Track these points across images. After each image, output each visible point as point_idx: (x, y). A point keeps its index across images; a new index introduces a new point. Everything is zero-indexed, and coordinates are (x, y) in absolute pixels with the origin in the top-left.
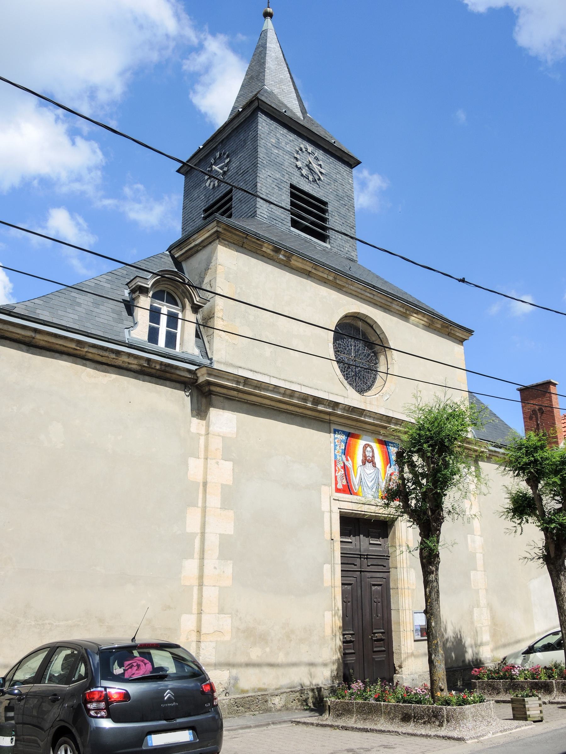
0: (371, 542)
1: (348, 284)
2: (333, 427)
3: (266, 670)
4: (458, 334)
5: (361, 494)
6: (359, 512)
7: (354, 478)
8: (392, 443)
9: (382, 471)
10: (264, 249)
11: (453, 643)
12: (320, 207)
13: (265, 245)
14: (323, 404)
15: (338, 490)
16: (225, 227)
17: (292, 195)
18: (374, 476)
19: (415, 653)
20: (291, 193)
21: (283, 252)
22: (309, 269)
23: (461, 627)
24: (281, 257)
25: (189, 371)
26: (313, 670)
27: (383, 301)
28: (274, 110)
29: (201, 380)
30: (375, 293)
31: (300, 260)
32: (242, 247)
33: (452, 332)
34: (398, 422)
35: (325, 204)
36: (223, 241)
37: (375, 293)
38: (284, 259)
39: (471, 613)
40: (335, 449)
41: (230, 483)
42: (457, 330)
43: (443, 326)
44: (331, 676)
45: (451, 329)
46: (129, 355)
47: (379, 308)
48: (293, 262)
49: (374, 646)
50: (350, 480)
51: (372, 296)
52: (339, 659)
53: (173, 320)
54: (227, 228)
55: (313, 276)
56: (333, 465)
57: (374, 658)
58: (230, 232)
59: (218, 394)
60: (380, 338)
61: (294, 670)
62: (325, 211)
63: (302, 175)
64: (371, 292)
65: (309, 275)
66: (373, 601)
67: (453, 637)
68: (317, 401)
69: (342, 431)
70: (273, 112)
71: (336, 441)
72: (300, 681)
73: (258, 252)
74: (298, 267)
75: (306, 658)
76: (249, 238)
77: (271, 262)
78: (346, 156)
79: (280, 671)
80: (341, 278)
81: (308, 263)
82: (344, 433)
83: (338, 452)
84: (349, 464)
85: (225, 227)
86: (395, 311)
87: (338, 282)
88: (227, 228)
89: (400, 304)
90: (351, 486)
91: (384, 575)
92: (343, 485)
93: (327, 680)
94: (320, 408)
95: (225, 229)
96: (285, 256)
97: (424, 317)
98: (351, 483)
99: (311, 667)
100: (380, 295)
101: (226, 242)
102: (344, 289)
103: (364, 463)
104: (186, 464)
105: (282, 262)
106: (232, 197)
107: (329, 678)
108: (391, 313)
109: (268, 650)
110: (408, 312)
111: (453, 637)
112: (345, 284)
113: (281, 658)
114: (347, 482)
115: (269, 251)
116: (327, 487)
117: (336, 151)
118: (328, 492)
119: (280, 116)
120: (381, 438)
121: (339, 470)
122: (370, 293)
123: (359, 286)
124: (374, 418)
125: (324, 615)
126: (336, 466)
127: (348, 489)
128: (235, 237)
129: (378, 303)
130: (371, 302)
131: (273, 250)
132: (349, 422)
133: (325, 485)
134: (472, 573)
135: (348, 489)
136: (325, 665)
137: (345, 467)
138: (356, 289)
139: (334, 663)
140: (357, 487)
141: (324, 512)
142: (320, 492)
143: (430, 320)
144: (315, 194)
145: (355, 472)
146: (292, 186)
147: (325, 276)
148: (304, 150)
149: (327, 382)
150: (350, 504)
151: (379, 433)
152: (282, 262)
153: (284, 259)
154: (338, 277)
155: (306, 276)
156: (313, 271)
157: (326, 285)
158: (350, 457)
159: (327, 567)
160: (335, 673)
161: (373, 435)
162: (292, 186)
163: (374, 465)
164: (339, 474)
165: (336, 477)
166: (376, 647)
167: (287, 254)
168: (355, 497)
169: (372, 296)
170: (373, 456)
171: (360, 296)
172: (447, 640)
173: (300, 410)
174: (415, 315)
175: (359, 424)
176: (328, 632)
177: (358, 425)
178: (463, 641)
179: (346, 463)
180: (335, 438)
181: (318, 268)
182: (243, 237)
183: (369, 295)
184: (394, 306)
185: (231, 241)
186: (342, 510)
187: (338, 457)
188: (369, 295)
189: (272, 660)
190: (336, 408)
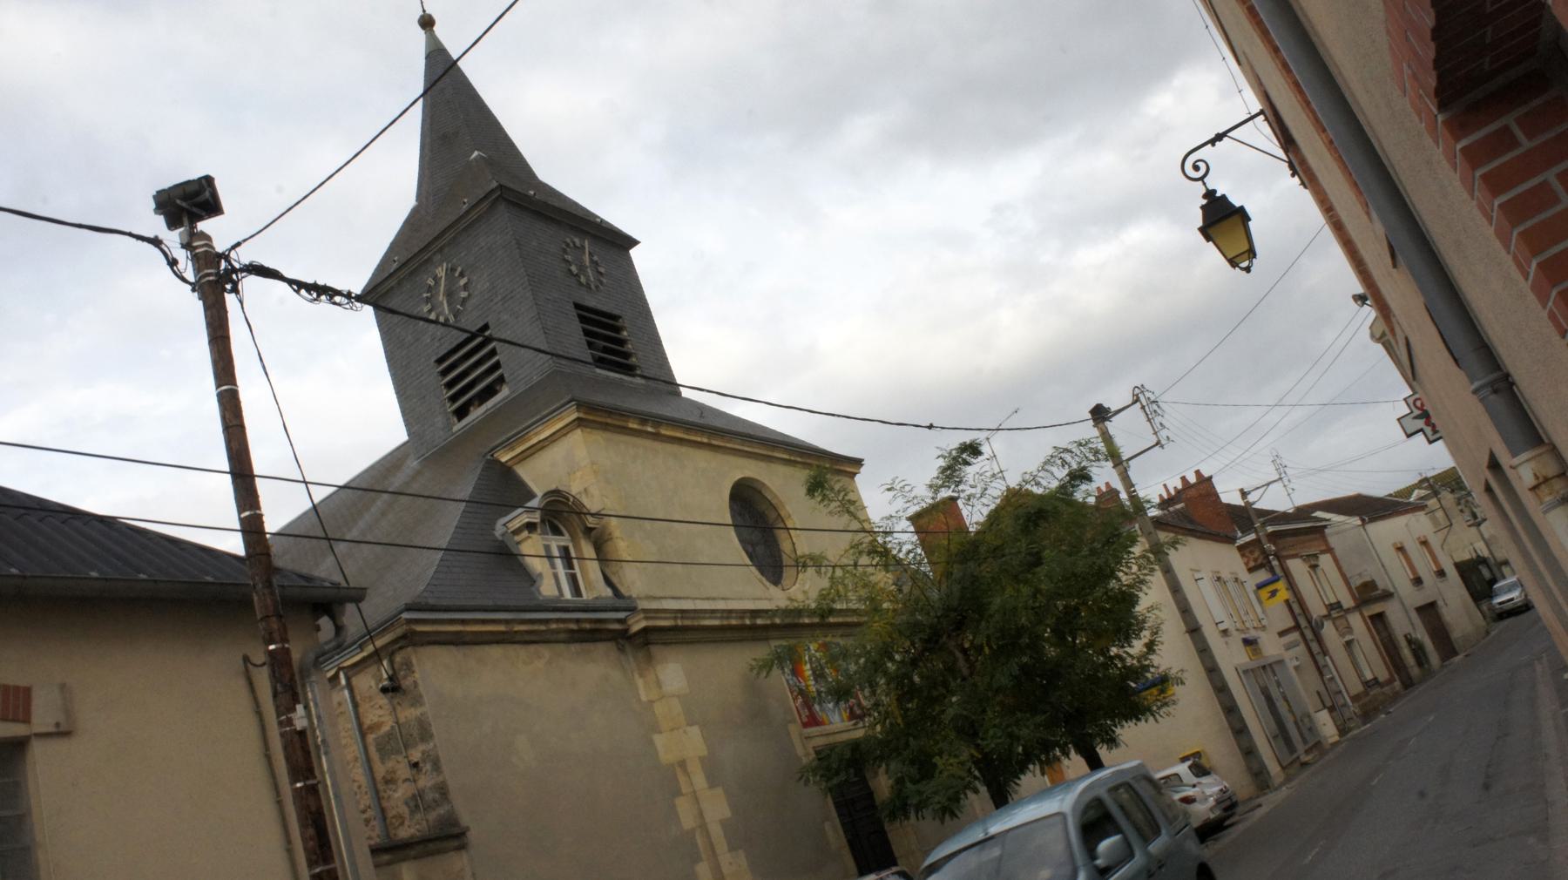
15: (805, 725)
17: (582, 319)
20: (580, 316)
25: (619, 621)
29: (636, 628)
35: (616, 318)
41: (705, 753)
46: (558, 621)
53: (1418, 581)
62: (618, 330)
63: (581, 284)
68: (755, 613)
94: (759, 621)
104: (651, 743)
106: (1410, 641)
118: (795, 729)
144: (605, 309)
146: (577, 306)
148: (1231, 585)
149: (740, 588)
159: (827, 826)
162: (577, 306)
172: (1066, 754)
173: (1525, 538)
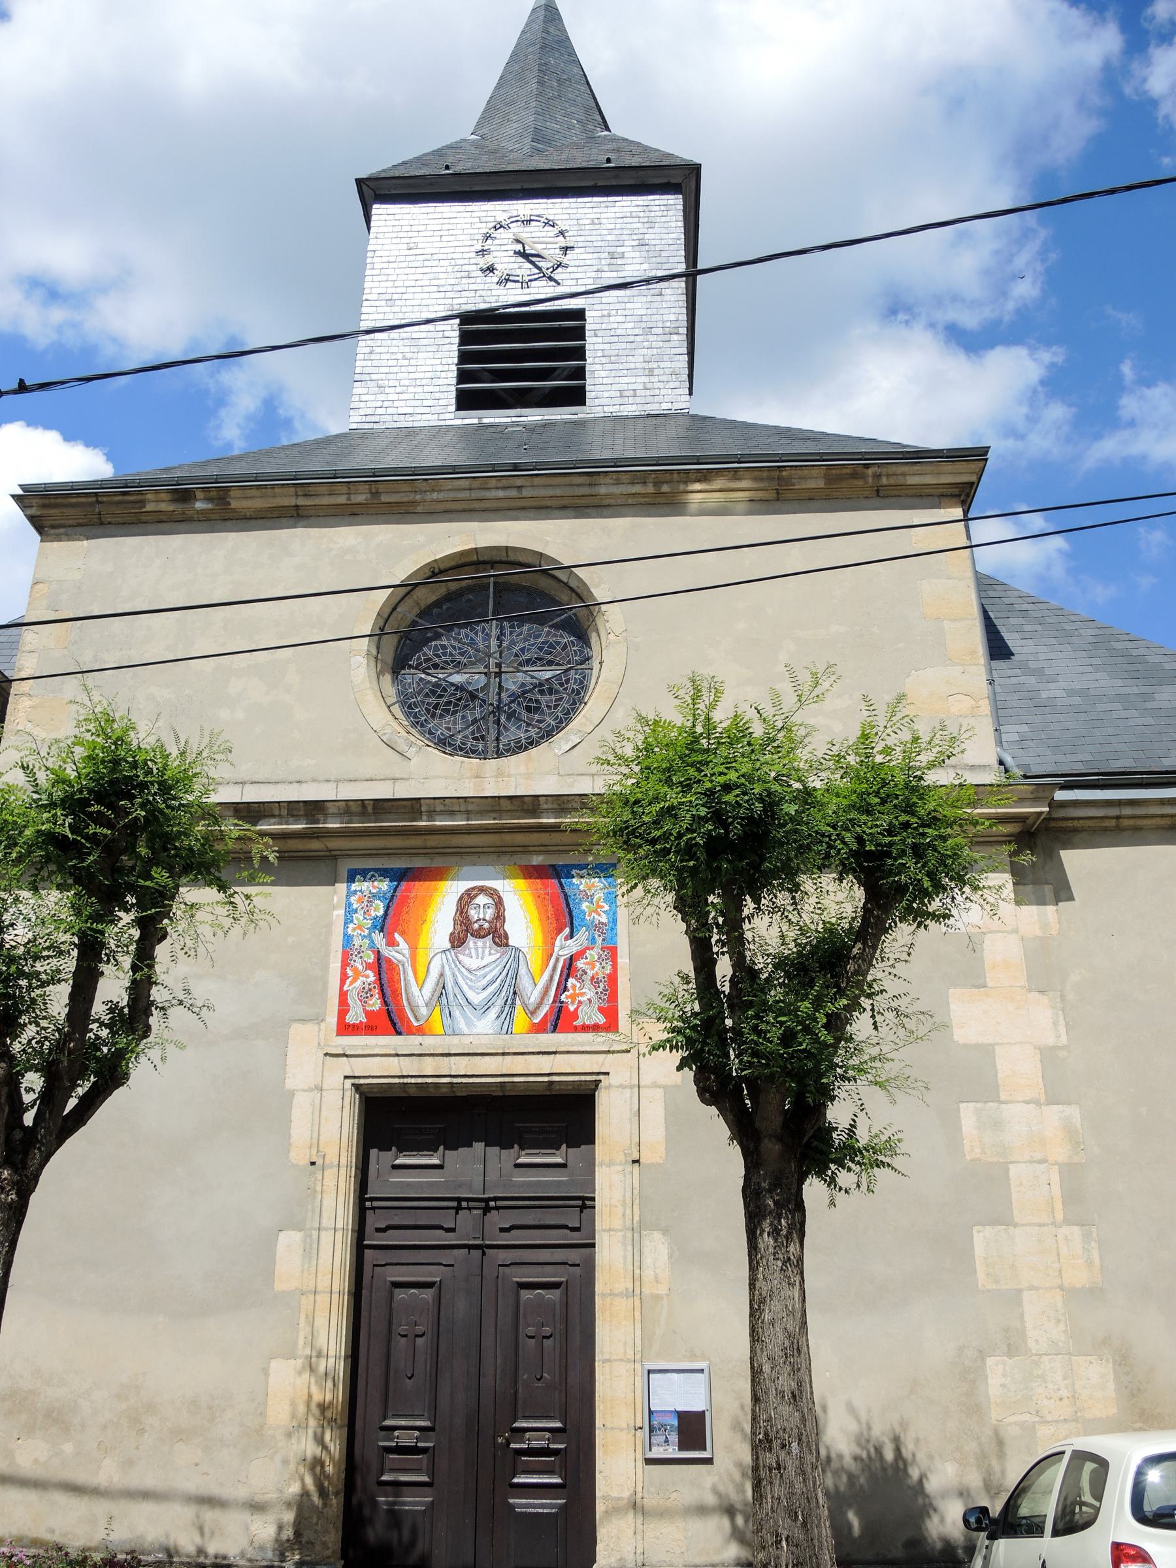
0: (521, 1160)
1: (421, 492)
2: (345, 866)
3: (61, 1498)
4: (912, 480)
5: (438, 1027)
6: (430, 1080)
7: (414, 989)
8: (580, 867)
9: (534, 957)
10: (149, 507)
11: (851, 1477)
12: (560, 328)
13: (149, 496)
14: (273, 816)
15: (345, 1029)
16: (40, 501)
18: (496, 972)
19: (650, 1501)
21: (199, 494)
22: (292, 502)
23: (904, 1425)
24: (199, 505)
26: (210, 1516)
27: (558, 492)
28: (408, 181)
30: (519, 482)
31: (254, 492)
32: (102, 524)
33: (884, 481)
34: (580, 802)
36: (53, 531)
37: (519, 482)
38: (210, 506)
39: (970, 1375)
40: (348, 921)
42: (906, 469)
43: (829, 480)
44: (276, 1540)
45: (878, 476)
47: (557, 512)
48: (234, 504)
49: (388, 1465)
50: (396, 994)
51: (513, 493)
52: (305, 1494)
54: (46, 501)
55: (312, 512)
56: (335, 966)
57: (513, 1507)
58: (56, 506)
59: (1075, 830)
60: (572, 589)
61: (147, 1508)
64: (504, 482)
65: (298, 515)
66: (521, 1336)
67: (856, 1458)
69: (376, 870)
70: (411, 186)
71: (353, 899)
72: (163, 1539)
73: (144, 518)
74: (261, 510)
75: (192, 1484)
76: (105, 499)
77: (182, 526)
78: (649, 172)
79: (101, 1508)
80: (391, 486)
81: (277, 490)
82: (384, 873)
83: (360, 927)
84: (399, 954)
85: (40, 501)
86: (620, 501)
87: (384, 498)
88: (46, 501)
89: (624, 477)
90: (402, 1011)
91: (573, 1255)
92: (368, 1014)
93: (262, 1548)
95: (44, 506)
96: (209, 500)
97: (740, 479)
98: (398, 1002)
99: (205, 1508)
100: (537, 480)
101: (62, 530)
102: (419, 509)
103: (457, 941)
105: (214, 516)
107: (270, 1545)
108: (605, 511)
109: (68, 1448)
110: (665, 488)
111: (856, 1458)
112: (411, 497)
113: (107, 1473)
114: (386, 1003)
115: (164, 507)
116: (310, 1027)
117: (616, 177)
119: (431, 184)
120: (537, 860)
121: (357, 974)
122: (504, 488)
123: (457, 483)
124: (468, 812)
125: (266, 1371)
126: (345, 963)
127: (391, 1019)
128: (70, 511)
129: (548, 503)
130: (523, 508)
131: (173, 501)
132: (397, 842)
133: (303, 1020)
134: (982, 1239)
135: (391, 1019)
136: (257, 1507)
137: (380, 965)
138: (452, 495)
139: (289, 1505)
140: (424, 1011)
141: (292, 1094)
142: (283, 1041)
143: (771, 479)
145: (421, 970)
147: (342, 499)
150: (388, 1061)
151: (525, 850)
152: (214, 516)
153: (210, 506)
154: (381, 487)
155: (291, 522)
156: (301, 501)
157: (358, 518)
158: (402, 934)
160: (288, 1533)
161: (505, 858)
163: (499, 937)
164: (358, 984)
165: (343, 996)
166: (392, 1470)
167: (214, 494)
168: (416, 1039)
169: (513, 493)
170: (500, 917)
171: (476, 505)
174: (697, 486)
175: (433, 841)
176: (279, 1413)
177: (429, 844)
178: (914, 1473)
179: (387, 952)
180: (349, 894)
181: (312, 489)
182: (91, 504)
183: (501, 494)
184: (603, 490)
185: (71, 522)
186: (362, 1081)
187: (357, 942)
188: (501, 494)
189: (80, 1476)
190: (321, 817)
